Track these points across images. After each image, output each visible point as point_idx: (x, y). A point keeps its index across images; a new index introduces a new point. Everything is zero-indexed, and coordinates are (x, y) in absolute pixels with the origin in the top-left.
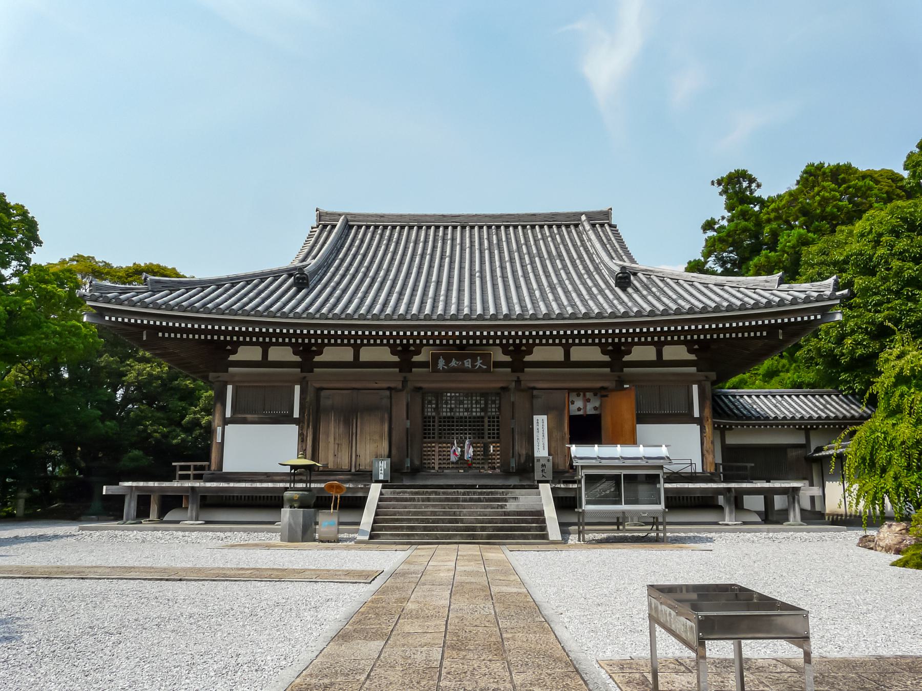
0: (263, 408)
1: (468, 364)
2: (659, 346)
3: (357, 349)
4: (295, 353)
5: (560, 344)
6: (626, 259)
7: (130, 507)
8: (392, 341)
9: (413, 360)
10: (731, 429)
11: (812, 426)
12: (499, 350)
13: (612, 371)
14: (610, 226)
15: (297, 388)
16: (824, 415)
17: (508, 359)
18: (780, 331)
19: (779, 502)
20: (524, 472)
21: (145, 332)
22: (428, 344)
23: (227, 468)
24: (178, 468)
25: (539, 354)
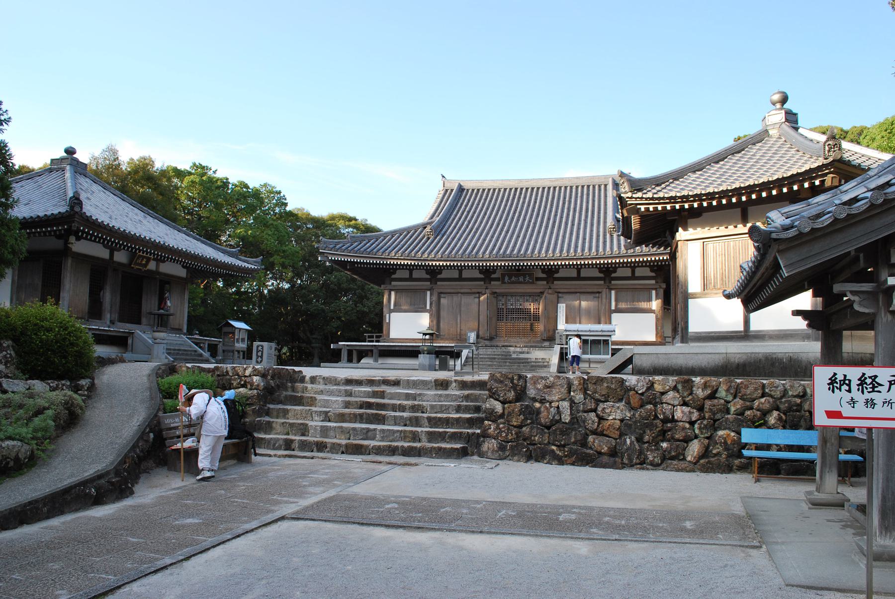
1: (521, 279)
15: (428, 293)
23: (391, 337)
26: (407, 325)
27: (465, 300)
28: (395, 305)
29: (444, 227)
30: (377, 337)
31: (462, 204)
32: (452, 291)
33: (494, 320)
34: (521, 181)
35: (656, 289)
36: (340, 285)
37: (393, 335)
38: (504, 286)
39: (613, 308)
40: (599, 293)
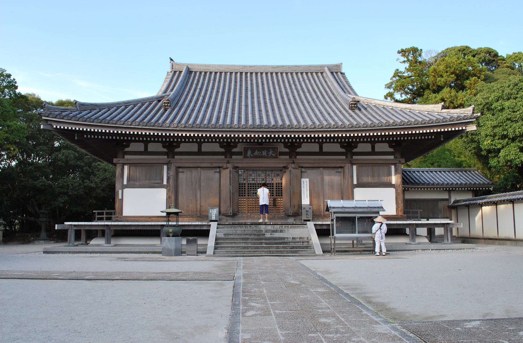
1: (264, 153)
3: (200, 145)
4: (164, 147)
5: (196, 142)
6: (352, 93)
7: (71, 235)
8: (199, 140)
9: (297, 151)
10: (408, 190)
11: (452, 189)
12: (282, 145)
13: (225, 158)
14: (341, 73)
15: (165, 167)
16: (459, 182)
17: (287, 150)
18: (442, 136)
19: (439, 231)
20: (296, 214)
21: (76, 135)
22: (243, 142)
23: (124, 214)
24: (96, 214)
26: (142, 202)
27: (205, 174)
28: (129, 180)
29: (181, 97)
30: (107, 214)
31: (192, 83)
32: (191, 165)
33: (236, 195)
34: (245, 66)
35: (395, 164)
36: (67, 162)
37: (127, 211)
38: (246, 160)
39: (355, 182)
40: (341, 167)
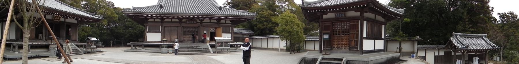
0: (154, 30)
2: (154, 19)
3: (210, 20)
25: (166, 20)
